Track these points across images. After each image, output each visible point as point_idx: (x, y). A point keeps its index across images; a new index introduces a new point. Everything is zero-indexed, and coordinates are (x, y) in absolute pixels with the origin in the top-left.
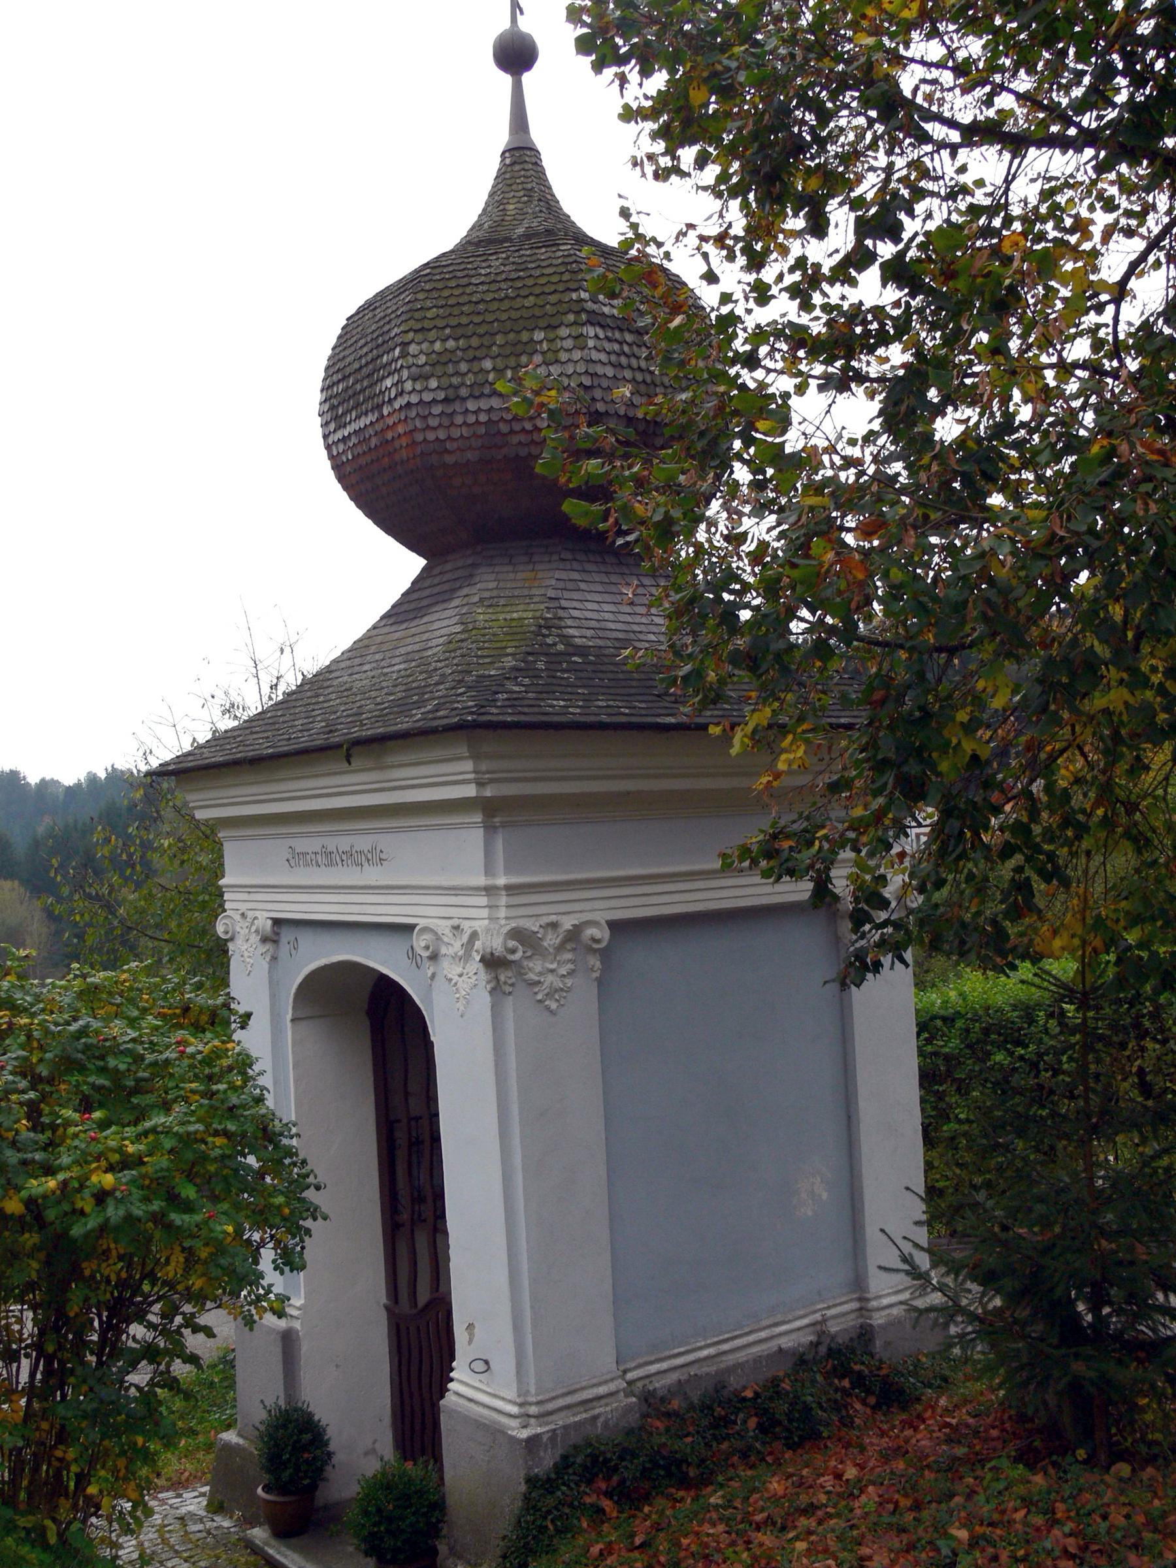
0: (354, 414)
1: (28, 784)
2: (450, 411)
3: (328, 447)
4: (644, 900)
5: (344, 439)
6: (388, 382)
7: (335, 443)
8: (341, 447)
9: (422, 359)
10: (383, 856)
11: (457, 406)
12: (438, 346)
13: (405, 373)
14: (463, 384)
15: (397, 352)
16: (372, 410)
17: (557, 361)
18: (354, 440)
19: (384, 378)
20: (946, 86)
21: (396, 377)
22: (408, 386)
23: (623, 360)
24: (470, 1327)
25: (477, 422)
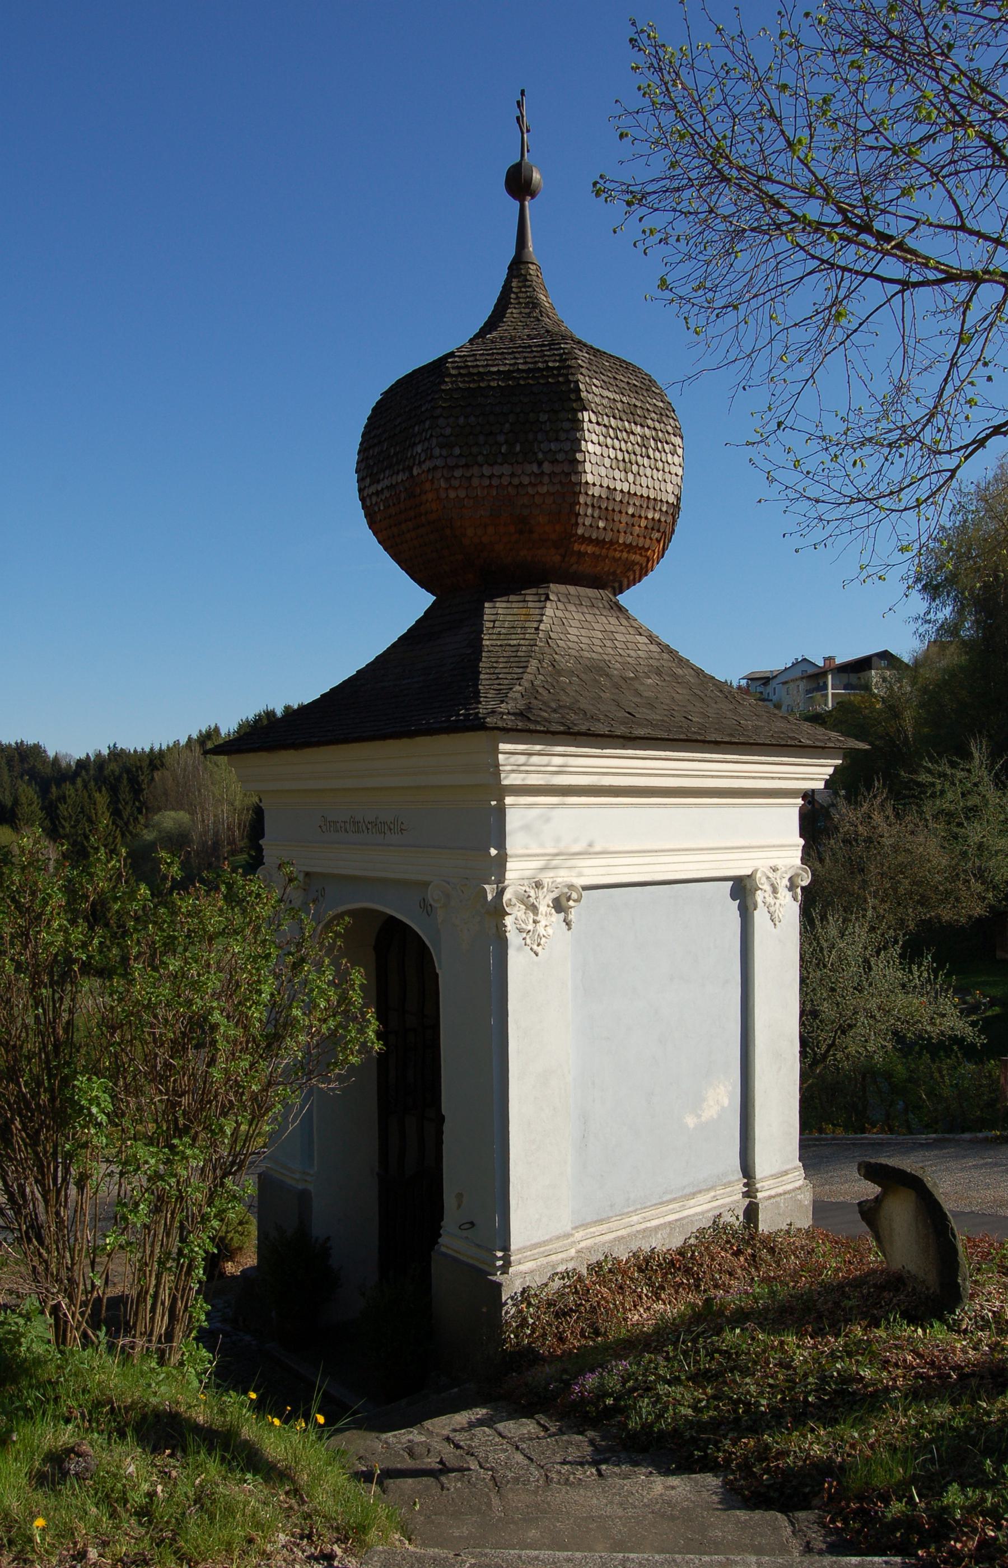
0: (387, 473)
1: (47, 757)
2: (468, 475)
3: (362, 499)
4: (631, 869)
5: (377, 493)
6: (419, 449)
7: (370, 496)
8: (374, 499)
9: (448, 431)
10: (403, 827)
11: (475, 470)
12: (461, 421)
13: (434, 441)
14: (480, 453)
15: (428, 423)
16: (403, 470)
17: (557, 440)
18: (386, 494)
19: (415, 444)
20: (872, 126)
21: (426, 444)
22: (437, 451)
23: (609, 441)
24: (460, 1196)
25: (490, 486)
